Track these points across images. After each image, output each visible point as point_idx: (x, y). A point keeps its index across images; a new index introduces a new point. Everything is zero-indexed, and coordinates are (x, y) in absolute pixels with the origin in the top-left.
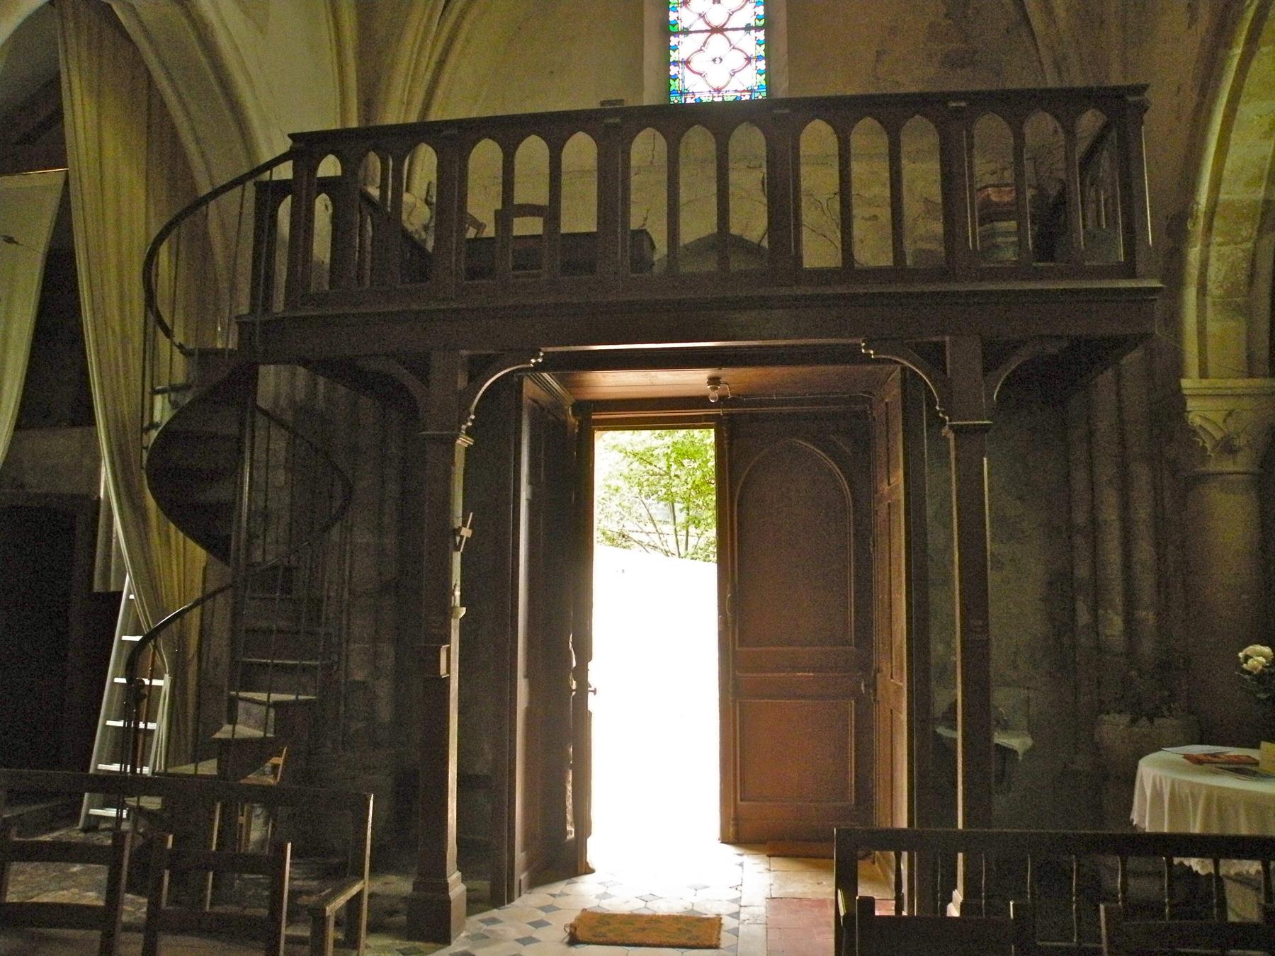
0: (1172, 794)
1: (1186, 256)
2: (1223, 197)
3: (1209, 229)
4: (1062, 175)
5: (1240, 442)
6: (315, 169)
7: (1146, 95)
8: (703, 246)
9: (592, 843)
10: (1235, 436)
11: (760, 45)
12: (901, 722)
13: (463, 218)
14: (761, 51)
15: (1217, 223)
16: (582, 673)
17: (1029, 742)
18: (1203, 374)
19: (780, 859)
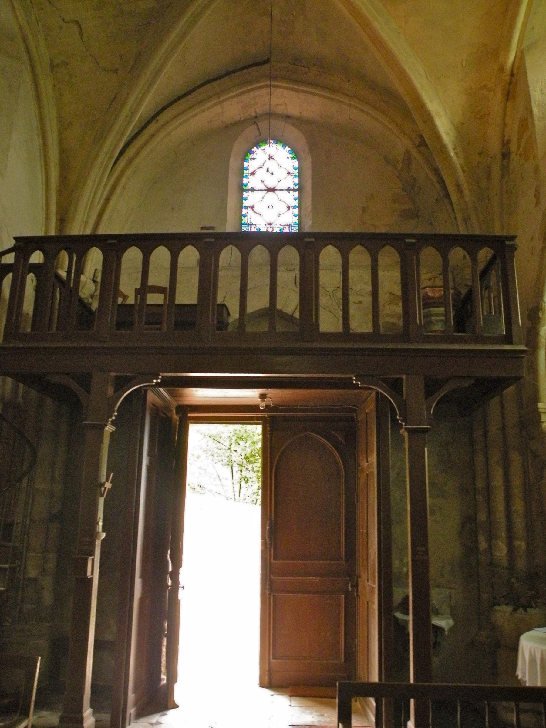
0: (542, 659)
1: (539, 331)
4: (470, 283)
6: (28, 259)
8: (261, 314)
9: (178, 687)
11: (296, 200)
12: (374, 610)
13: (117, 292)
14: (296, 203)
16: (175, 575)
17: (451, 622)
19: (298, 698)
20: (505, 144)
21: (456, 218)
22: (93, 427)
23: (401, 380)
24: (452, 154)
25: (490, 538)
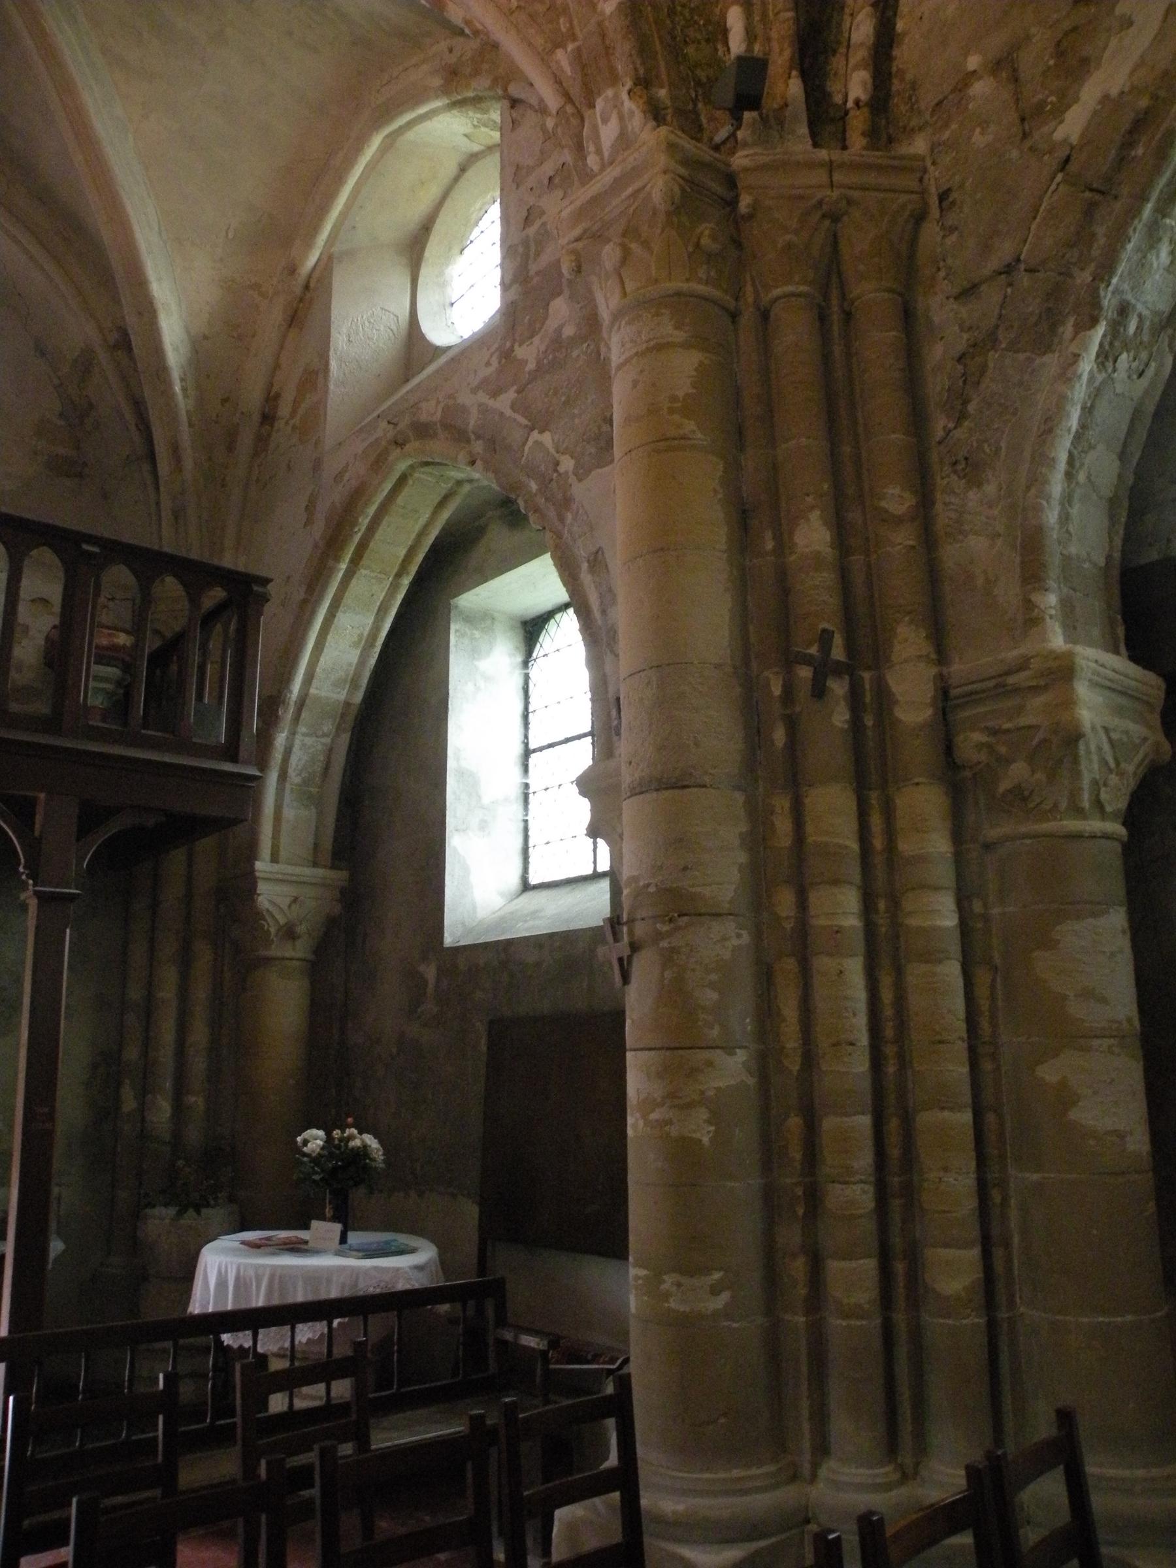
0: (237, 1278)
1: (274, 739)
2: (313, 691)
5: (301, 929)
7: (270, 587)
10: (298, 923)
15: (304, 715)
18: (275, 859)
20: (272, 399)
21: (158, 504)
23: (35, 799)
24: (177, 388)
25: (144, 1091)
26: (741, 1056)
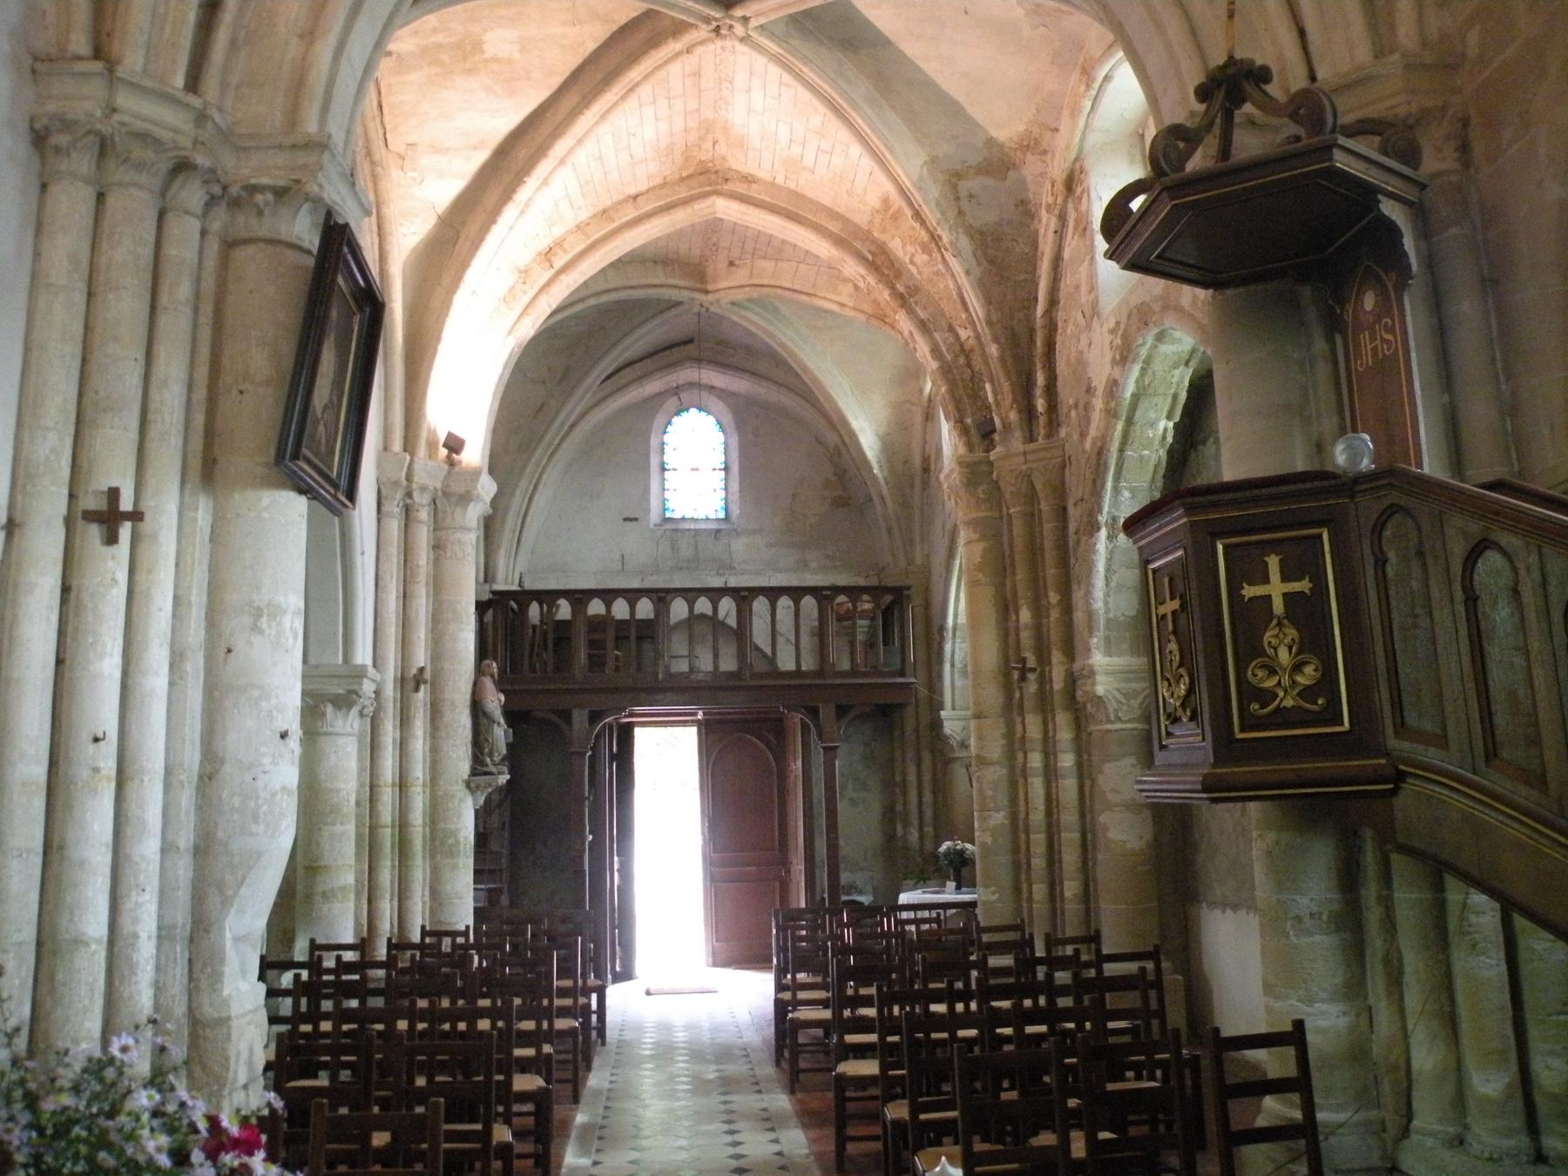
3: (954, 635)
15: (958, 633)
18: (954, 709)
22: (577, 753)
26: (1002, 814)
